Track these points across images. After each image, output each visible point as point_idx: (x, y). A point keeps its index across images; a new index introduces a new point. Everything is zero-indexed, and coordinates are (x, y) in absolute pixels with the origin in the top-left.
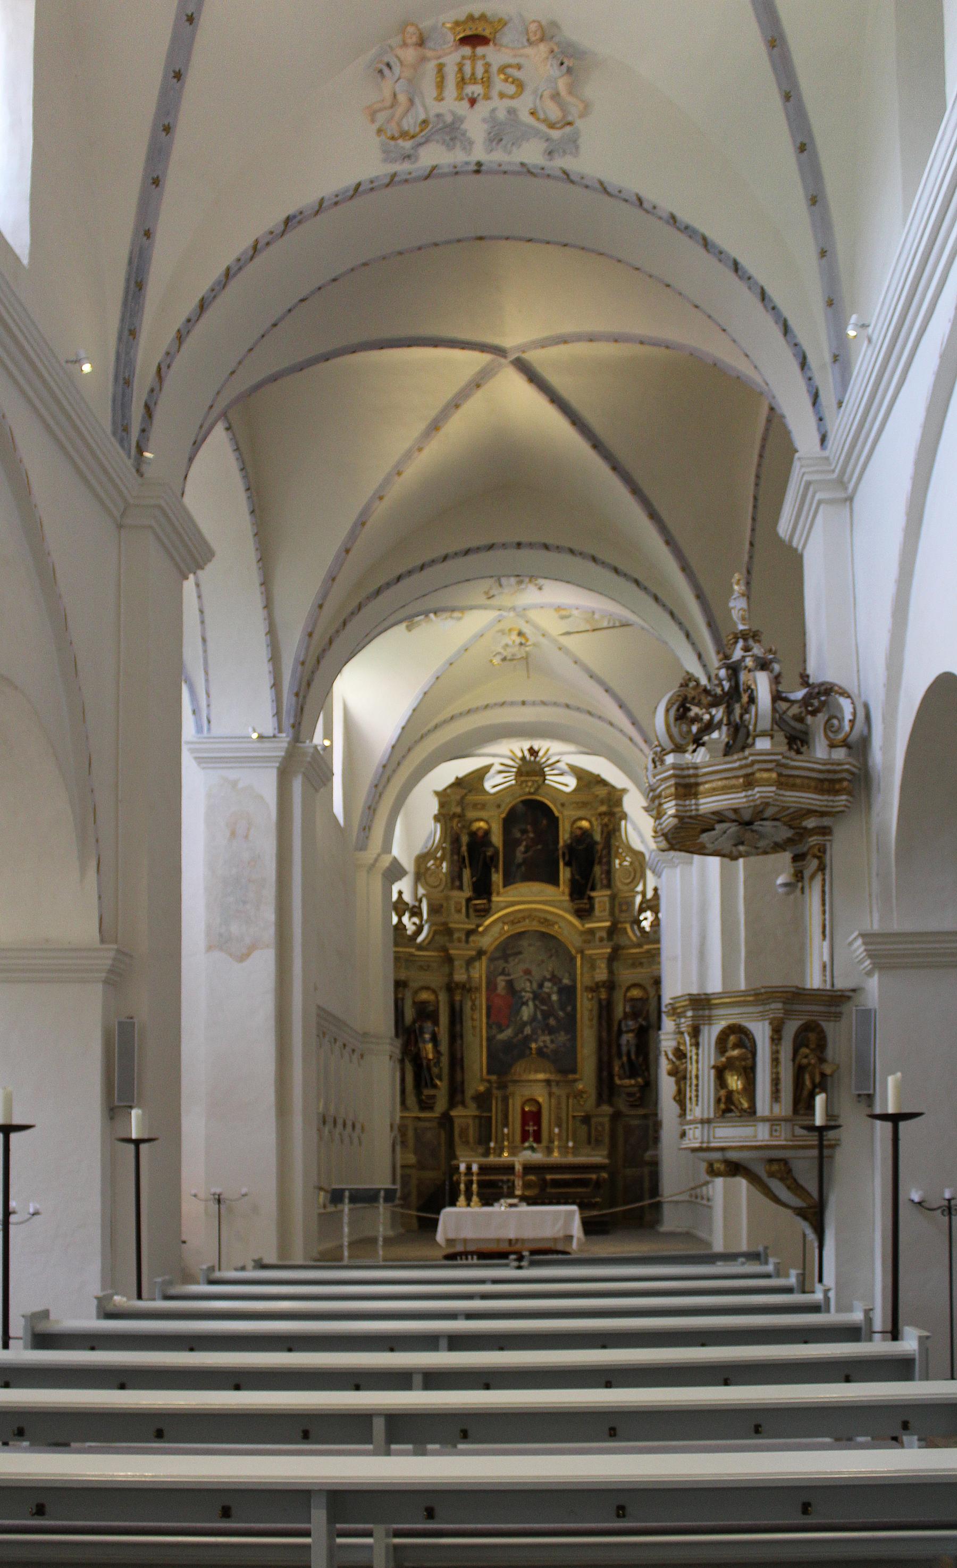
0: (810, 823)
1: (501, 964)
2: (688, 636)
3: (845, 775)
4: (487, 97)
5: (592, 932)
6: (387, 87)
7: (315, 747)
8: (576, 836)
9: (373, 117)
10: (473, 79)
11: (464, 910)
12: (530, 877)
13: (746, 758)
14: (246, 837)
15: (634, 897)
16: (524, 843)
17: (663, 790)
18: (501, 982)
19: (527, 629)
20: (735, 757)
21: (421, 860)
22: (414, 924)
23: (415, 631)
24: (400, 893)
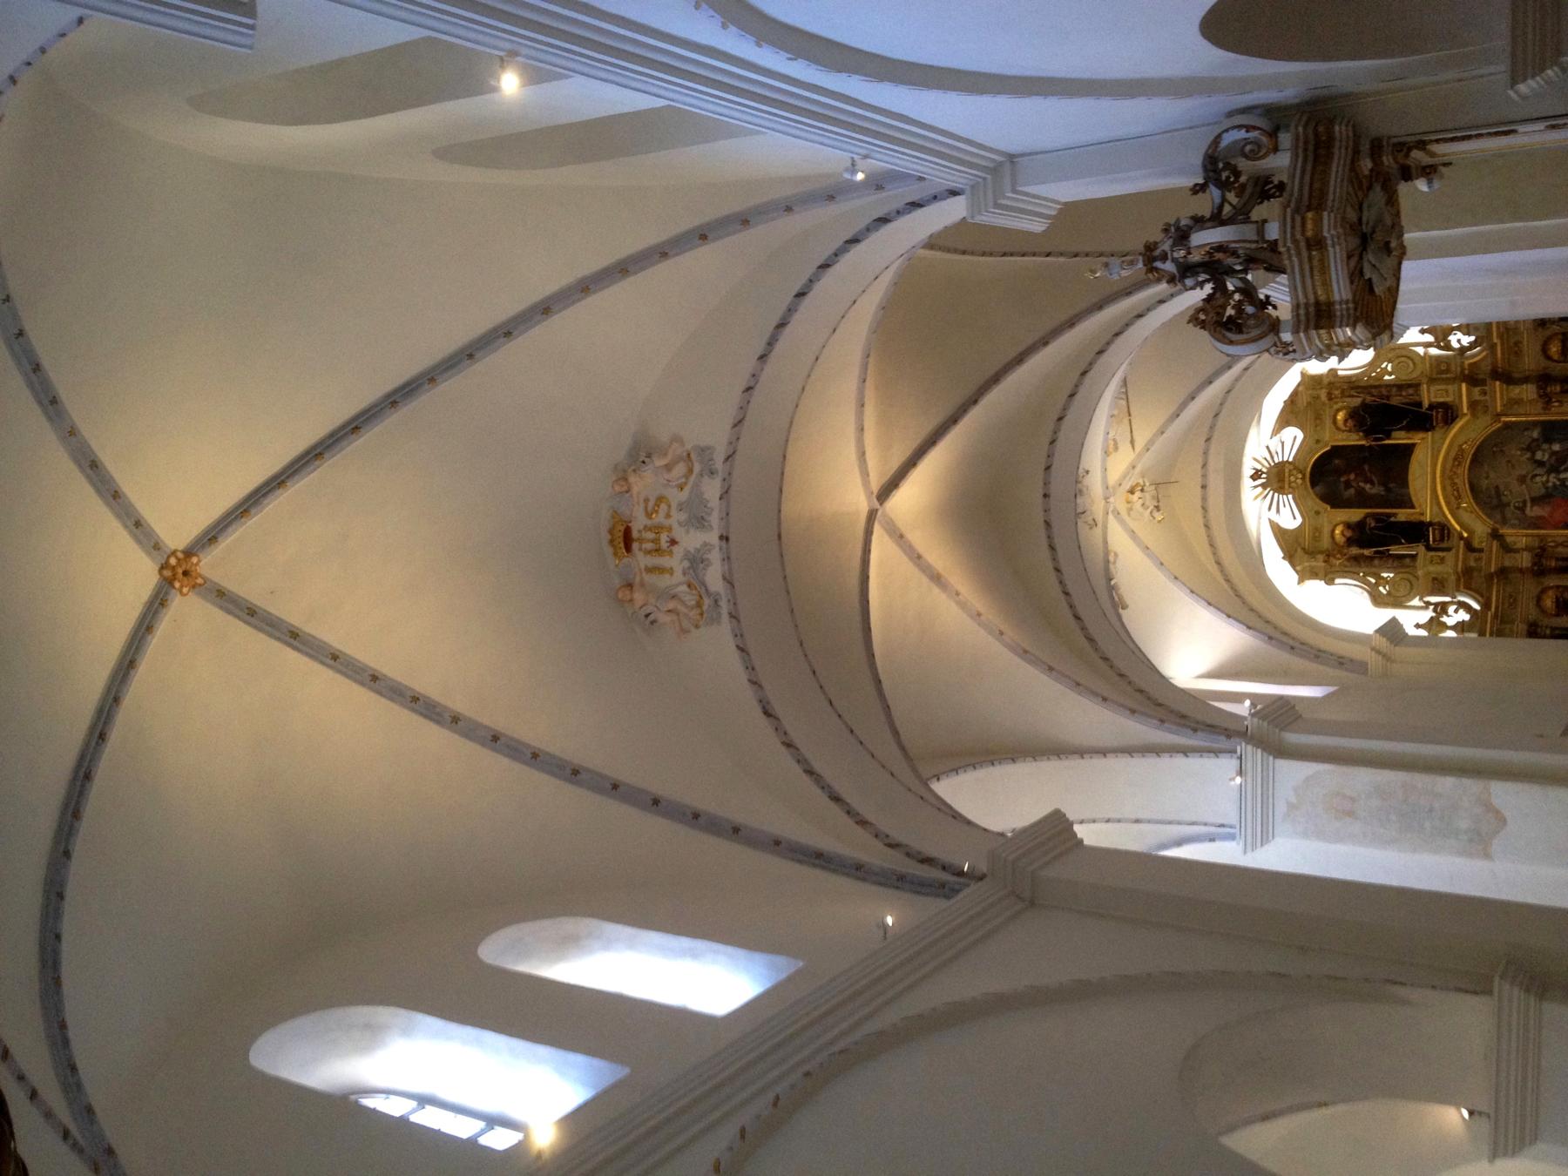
0: (1366, 165)
1: (1509, 512)
2: (1140, 316)
3: (1310, 131)
4: (670, 529)
5: (1473, 405)
6: (664, 618)
7: (1252, 715)
8: (1355, 426)
9: (684, 631)
10: (656, 541)
11: (1441, 554)
12: (1404, 482)
13: (1288, 250)
14: (1353, 800)
15: (1431, 357)
16: (1361, 484)
17: (1321, 341)
18: (1533, 511)
19: (1127, 486)
20: (1286, 262)
21: (1378, 601)
22: (1456, 611)
23: (1128, 600)
24: (1418, 626)
